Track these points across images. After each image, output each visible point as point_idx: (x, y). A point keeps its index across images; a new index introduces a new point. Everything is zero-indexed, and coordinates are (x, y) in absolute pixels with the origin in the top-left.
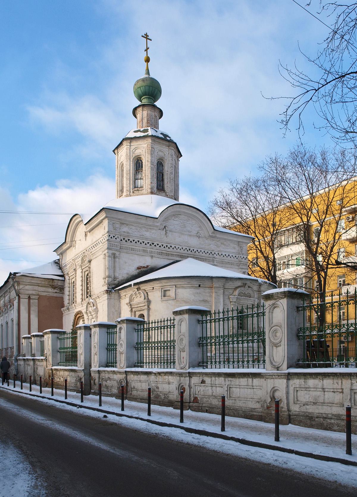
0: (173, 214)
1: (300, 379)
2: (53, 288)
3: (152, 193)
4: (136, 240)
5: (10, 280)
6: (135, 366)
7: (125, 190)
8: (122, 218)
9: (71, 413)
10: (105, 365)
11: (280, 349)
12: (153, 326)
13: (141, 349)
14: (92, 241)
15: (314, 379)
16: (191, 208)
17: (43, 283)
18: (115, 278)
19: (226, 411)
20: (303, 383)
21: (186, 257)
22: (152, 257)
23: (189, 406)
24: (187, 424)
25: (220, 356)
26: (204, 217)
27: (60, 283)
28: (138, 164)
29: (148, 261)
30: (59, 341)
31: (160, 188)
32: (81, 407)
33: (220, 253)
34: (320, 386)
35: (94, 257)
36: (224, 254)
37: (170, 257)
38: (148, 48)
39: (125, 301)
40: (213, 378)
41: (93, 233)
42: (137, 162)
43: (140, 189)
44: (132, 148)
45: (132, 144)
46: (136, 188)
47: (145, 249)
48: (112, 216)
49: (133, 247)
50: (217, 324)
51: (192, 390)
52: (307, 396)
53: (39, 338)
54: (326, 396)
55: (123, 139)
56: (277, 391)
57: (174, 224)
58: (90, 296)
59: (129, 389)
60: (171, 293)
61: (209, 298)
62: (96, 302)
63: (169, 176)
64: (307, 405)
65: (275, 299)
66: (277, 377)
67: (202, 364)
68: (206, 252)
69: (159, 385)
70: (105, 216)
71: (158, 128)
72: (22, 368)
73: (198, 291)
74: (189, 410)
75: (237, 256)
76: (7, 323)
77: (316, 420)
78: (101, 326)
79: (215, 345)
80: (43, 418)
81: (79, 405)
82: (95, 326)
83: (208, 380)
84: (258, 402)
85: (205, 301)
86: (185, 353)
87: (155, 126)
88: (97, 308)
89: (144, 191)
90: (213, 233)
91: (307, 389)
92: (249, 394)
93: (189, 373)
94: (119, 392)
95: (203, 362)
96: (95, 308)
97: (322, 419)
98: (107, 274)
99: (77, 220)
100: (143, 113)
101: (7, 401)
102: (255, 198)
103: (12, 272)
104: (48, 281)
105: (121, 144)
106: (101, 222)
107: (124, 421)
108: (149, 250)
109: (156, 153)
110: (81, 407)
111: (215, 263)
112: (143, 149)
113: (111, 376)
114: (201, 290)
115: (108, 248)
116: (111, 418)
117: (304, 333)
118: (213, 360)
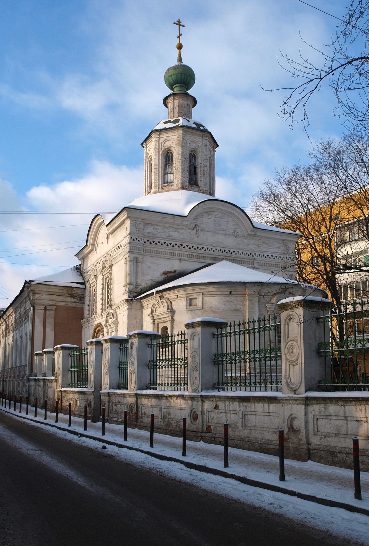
1: (320, 404)
2: (72, 297)
3: (183, 188)
4: (162, 242)
5: (26, 289)
6: (147, 388)
7: (153, 185)
9: (69, 443)
10: (145, 387)
11: (297, 368)
12: (180, 339)
13: (154, 368)
14: (114, 243)
15: (335, 404)
16: (226, 204)
17: (61, 291)
18: (137, 285)
19: (230, 442)
20: (323, 410)
21: (218, 259)
22: (180, 260)
23: (202, 437)
24: (190, 458)
25: (255, 376)
26: (242, 213)
27: (80, 292)
28: (168, 158)
29: (175, 265)
30: (70, 358)
32: (83, 435)
33: (261, 254)
34: (341, 414)
35: (116, 261)
36: (266, 255)
37: (203, 260)
38: (180, 35)
39: (147, 311)
40: (227, 403)
41: (115, 235)
43: (170, 184)
44: (162, 140)
45: (161, 136)
46: (165, 184)
47: (172, 251)
50: (242, 336)
51: (205, 416)
52: (328, 426)
53: (51, 355)
54: (349, 426)
55: (152, 132)
56: (296, 420)
57: (206, 222)
58: (111, 306)
59: (140, 415)
60: (198, 302)
61: (241, 307)
62: (116, 313)
63: (202, 169)
64: (329, 437)
65: (290, 309)
66: (294, 402)
67: (218, 385)
68: (244, 253)
69: (171, 412)
70: (126, 216)
71: (191, 117)
72: (32, 390)
73: (228, 299)
74: (202, 441)
75: (282, 257)
76: (22, 338)
77: (339, 455)
79: (250, 362)
80: (34, 448)
81: (80, 434)
82: (106, 341)
83: (221, 405)
84: (275, 432)
85: (237, 311)
86: (198, 373)
87: (187, 115)
88: (117, 319)
89: (175, 187)
90: (252, 231)
91: (328, 417)
92: (266, 421)
93: (201, 396)
95: (218, 384)
96: (114, 319)
97: (344, 455)
98: (128, 281)
99: (99, 221)
100: (174, 103)
101: (7, 428)
102: (307, 188)
103: (28, 280)
104: (67, 289)
105: (149, 136)
106: (123, 223)
107: (124, 453)
108: (176, 252)
109: (188, 145)
110: (83, 435)
111: (256, 266)
112: (173, 141)
113: (121, 399)
114: (232, 298)
115: (129, 252)
116: (111, 449)
118: (248, 381)
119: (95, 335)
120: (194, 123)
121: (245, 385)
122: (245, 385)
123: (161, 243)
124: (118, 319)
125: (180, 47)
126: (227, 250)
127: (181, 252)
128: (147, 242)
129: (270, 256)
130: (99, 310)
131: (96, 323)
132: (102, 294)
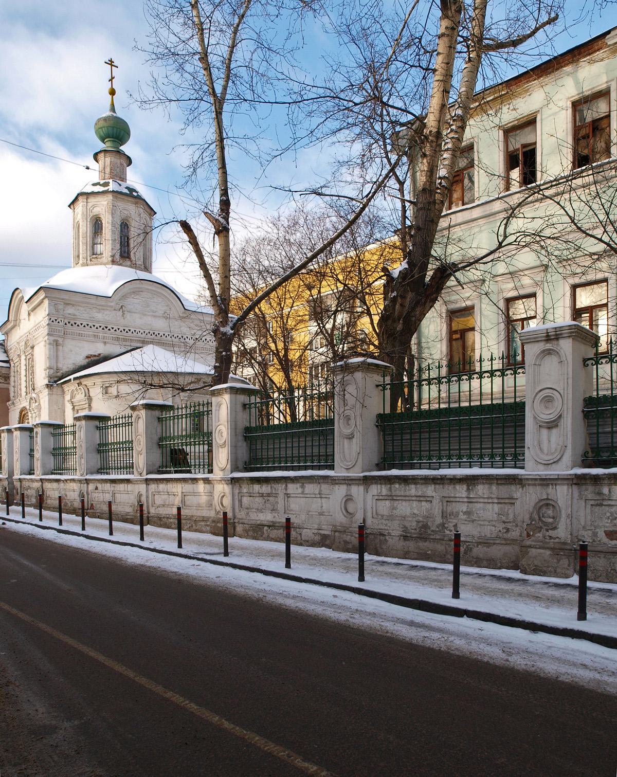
0: (132, 291)
3: (113, 262)
4: (85, 323)
6: (52, 474)
7: (81, 256)
8: (67, 298)
10: (27, 473)
12: (124, 421)
18: (58, 370)
21: (145, 343)
22: (105, 343)
26: (172, 293)
28: (97, 225)
29: (100, 349)
30: (98, 432)
31: (124, 255)
37: (128, 343)
38: (113, 78)
42: (95, 222)
43: (99, 256)
44: (90, 205)
45: (89, 201)
46: (94, 255)
48: (54, 296)
49: (80, 332)
55: (78, 195)
57: (134, 303)
58: (34, 390)
62: (39, 397)
69: (67, 493)
70: (44, 295)
78: (43, 425)
82: (16, 429)
83: (99, 486)
84: (131, 506)
88: (39, 404)
89: (104, 260)
92: (126, 499)
93: (86, 479)
94: (37, 502)
98: (48, 365)
106: (42, 302)
108: (101, 335)
112: (102, 206)
115: (48, 334)
117: (174, 441)
119: (21, 420)
120: (127, 188)
121: (199, 467)
122: (199, 467)
123: (83, 325)
124: (41, 403)
125: (112, 92)
126: (156, 333)
127: (105, 335)
128: (67, 323)
130: (24, 394)
131: (22, 406)
132: (26, 376)
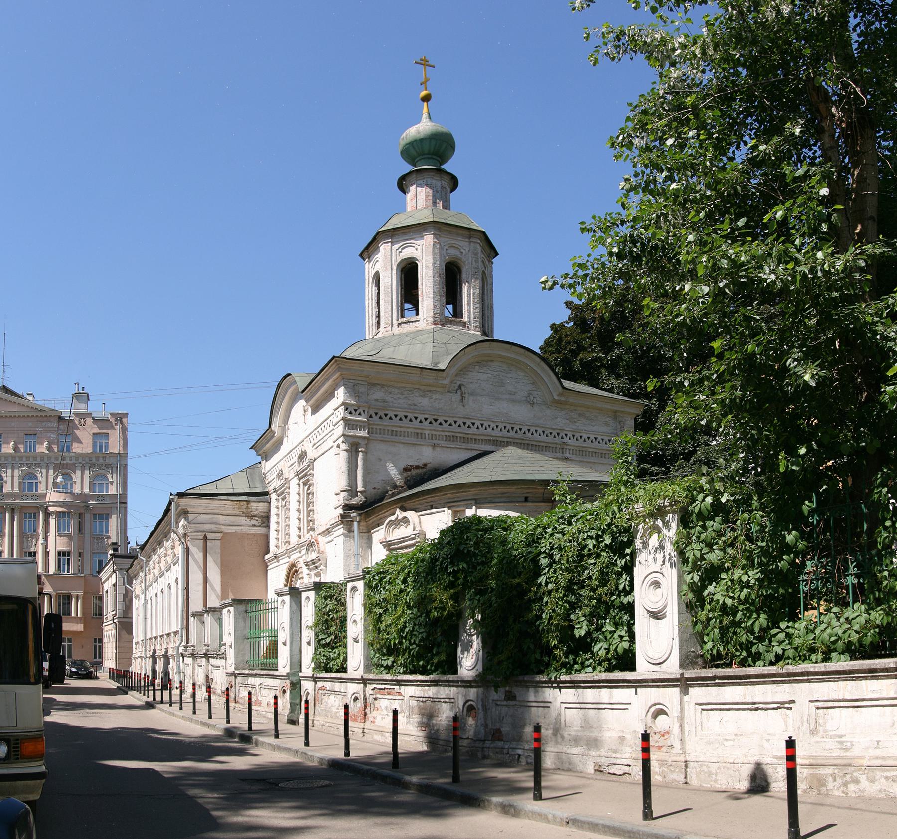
36: (585, 436)
108: (427, 432)
111: (567, 455)
128: (374, 415)
129: (592, 437)
